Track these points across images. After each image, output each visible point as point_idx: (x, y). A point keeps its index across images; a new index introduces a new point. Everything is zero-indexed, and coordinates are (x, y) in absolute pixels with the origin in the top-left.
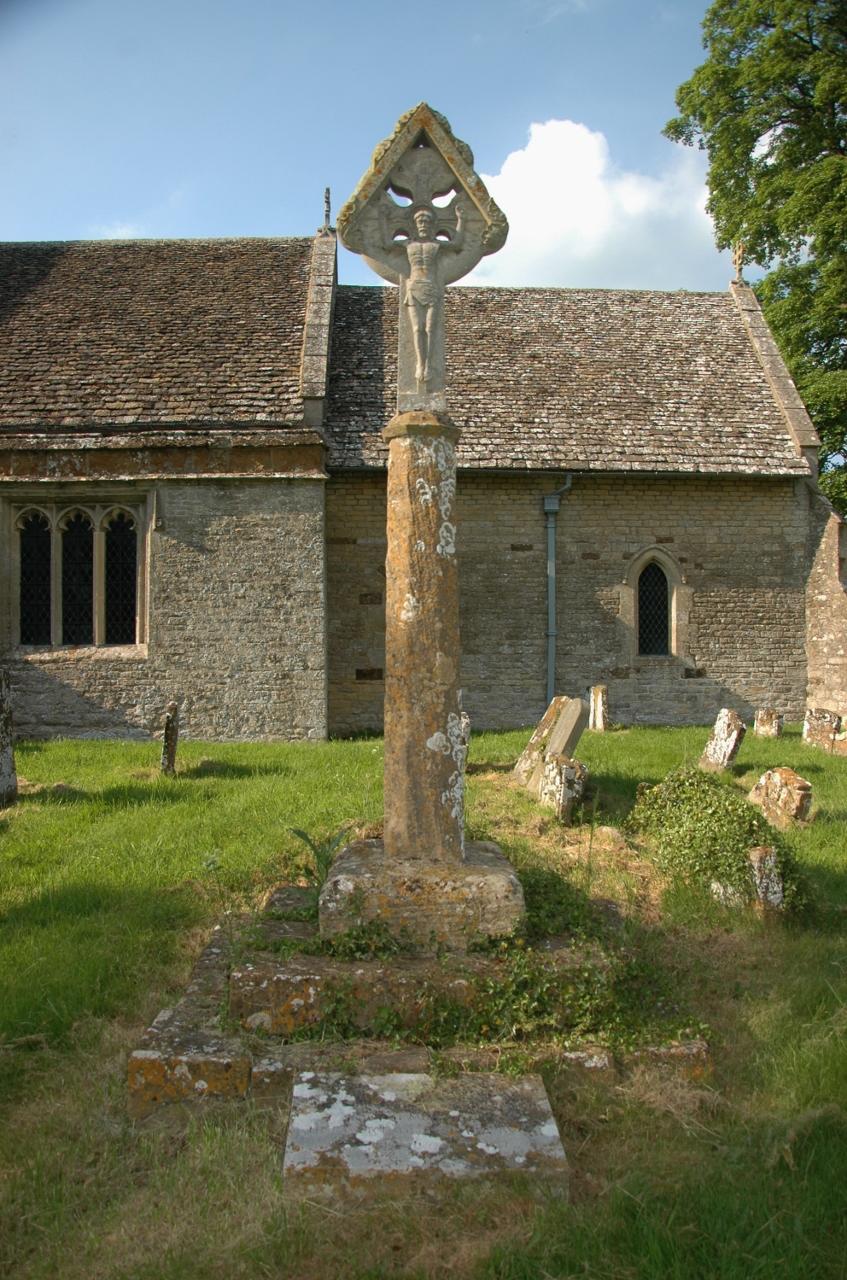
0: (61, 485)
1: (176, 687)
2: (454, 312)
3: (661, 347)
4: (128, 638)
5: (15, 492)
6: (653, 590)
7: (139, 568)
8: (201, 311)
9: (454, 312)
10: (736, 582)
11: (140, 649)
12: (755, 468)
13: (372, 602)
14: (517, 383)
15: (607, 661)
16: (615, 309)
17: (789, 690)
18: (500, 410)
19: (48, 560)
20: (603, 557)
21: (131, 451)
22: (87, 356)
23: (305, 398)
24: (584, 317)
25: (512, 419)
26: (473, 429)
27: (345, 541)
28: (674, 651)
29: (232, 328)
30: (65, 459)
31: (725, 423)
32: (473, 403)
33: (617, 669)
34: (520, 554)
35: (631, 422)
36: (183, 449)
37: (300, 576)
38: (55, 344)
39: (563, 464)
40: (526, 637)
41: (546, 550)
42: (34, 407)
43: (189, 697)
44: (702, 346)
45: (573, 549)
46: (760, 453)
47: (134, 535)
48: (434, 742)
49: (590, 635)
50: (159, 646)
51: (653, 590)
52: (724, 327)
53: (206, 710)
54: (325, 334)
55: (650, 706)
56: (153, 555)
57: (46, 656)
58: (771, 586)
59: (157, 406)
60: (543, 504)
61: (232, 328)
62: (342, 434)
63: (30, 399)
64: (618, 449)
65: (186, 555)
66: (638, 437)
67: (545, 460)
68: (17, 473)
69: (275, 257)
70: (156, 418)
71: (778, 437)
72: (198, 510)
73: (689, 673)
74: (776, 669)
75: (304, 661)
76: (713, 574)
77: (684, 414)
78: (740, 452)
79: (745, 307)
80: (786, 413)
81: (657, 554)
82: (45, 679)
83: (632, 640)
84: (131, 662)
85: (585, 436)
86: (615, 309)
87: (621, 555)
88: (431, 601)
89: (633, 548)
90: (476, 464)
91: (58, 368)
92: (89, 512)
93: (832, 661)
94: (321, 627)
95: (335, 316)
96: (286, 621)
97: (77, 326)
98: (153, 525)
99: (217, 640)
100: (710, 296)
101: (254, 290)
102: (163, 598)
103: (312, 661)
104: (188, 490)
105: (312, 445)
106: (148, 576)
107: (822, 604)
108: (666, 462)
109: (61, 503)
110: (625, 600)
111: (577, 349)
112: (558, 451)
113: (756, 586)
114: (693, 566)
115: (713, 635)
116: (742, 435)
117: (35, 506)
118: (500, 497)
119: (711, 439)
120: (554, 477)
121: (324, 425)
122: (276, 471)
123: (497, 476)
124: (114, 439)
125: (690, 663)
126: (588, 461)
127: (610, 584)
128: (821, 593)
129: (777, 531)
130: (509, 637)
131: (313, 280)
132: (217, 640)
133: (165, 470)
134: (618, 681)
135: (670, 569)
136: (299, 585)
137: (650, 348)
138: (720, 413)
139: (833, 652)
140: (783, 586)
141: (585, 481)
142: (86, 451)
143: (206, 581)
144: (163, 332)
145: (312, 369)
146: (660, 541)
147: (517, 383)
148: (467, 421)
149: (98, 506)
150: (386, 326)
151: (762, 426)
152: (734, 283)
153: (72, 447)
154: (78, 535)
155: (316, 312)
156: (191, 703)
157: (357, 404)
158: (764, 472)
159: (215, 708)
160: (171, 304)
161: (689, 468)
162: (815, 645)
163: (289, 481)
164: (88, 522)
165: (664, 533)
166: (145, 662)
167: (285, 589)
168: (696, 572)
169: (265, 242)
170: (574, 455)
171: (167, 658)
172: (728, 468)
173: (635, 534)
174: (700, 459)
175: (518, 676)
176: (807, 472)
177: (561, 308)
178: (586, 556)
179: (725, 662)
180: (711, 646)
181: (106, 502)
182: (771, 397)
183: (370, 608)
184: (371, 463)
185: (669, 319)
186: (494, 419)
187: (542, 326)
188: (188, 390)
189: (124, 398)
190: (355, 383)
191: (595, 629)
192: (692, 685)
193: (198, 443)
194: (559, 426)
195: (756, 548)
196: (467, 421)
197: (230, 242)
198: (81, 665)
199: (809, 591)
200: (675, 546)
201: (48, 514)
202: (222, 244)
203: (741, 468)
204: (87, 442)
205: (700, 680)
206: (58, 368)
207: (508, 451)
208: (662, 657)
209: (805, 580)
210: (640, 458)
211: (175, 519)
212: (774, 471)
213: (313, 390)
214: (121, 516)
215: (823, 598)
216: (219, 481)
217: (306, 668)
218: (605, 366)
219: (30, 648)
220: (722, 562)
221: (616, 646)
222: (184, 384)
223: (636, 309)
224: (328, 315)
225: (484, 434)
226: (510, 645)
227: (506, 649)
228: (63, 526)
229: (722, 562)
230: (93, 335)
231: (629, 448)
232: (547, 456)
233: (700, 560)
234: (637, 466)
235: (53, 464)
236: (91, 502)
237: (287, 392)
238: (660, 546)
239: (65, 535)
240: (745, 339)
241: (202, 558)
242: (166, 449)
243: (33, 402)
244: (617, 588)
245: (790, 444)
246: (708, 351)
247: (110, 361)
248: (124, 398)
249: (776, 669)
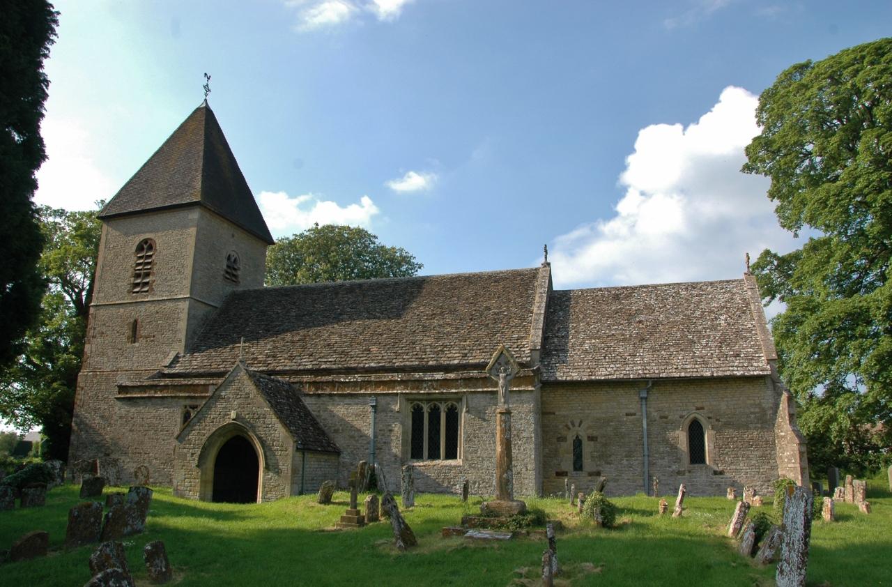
0: (428, 394)
1: (474, 477)
2: (604, 301)
3: (703, 312)
4: (454, 457)
5: (411, 397)
6: (696, 432)
7: (459, 427)
8: (488, 308)
9: (604, 301)
10: (738, 427)
11: (459, 461)
12: (742, 372)
13: (562, 441)
14: (631, 336)
15: (674, 467)
16: (683, 293)
17: (769, 481)
18: (621, 350)
19: (423, 424)
20: (669, 417)
21: (456, 380)
22: (439, 333)
23: (531, 350)
24: (667, 299)
25: (626, 354)
26: (607, 360)
27: (550, 413)
28: (707, 462)
29: (501, 317)
30: (430, 383)
31: (730, 350)
32: (608, 347)
33: (679, 471)
34: (630, 417)
35: (683, 353)
36: (476, 379)
37: (524, 431)
38: (425, 327)
39: (647, 376)
40: (634, 456)
41: (642, 415)
42: (417, 357)
43: (479, 482)
44: (725, 309)
45: (655, 415)
46: (745, 365)
47: (457, 413)
48: (505, 476)
49: (665, 455)
50: (467, 460)
51: (696, 432)
52: (737, 298)
53: (486, 487)
54: (542, 316)
55: (697, 489)
56: (464, 423)
57: (421, 464)
58: (756, 428)
59: (468, 355)
60: (640, 394)
61: (501, 317)
62: (548, 365)
63: (415, 353)
64: (675, 367)
65: (478, 422)
66: (685, 360)
67: (639, 374)
68: (411, 389)
69: (522, 280)
70: (467, 361)
71: (757, 355)
72: (483, 403)
73: (715, 473)
74: (761, 470)
75: (526, 467)
76: (725, 424)
77: (710, 347)
78: (736, 364)
79: (749, 287)
80: (762, 343)
81: (697, 416)
82: (420, 473)
83: (686, 458)
84: (455, 467)
85: (660, 361)
86: (683, 293)
87: (678, 416)
88: (504, 447)
89: (685, 413)
90: (607, 377)
91: (427, 338)
92: (439, 404)
93: (789, 466)
94: (533, 453)
95: (548, 306)
96: (519, 450)
97: (434, 318)
98: (464, 410)
99: (490, 458)
100: (733, 282)
101: (512, 297)
102: (468, 440)
103: (529, 467)
104: (479, 395)
105: (528, 376)
106: (462, 431)
107: (782, 437)
108: (697, 371)
109: (428, 401)
110: (681, 438)
111: (661, 316)
112: (646, 369)
113: (748, 428)
114: (714, 420)
115: (727, 453)
116: (738, 355)
117: (418, 402)
118: (620, 391)
119: (722, 359)
120: (645, 381)
121: (540, 361)
122: (514, 387)
123: (618, 382)
124: (449, 375)
125: (716, 468)
126: (660, 373)
127: (674, 430)
128: (782, 432)
129: (757, 402)
130: (626, 456)
131: (539, 290)
132: (490, 458)
133: (470, 387)
134: (680, 477)
135: (703, 421)
136: (524, 434)
137: (698, 313)
138: (728, 345)
139: (789, 461)
140: (762, 428)
141: (658, 383)
142: (438, 380)
143: (486, 433)
144: (471, 319)
145: (535, 336)
146: (697, 409)
147: (631, 336)
148: (605, 357)
149: (443, 403)
150: (572, 310)
151: (749, 350)
152: (745, 274)
153: (433, 378)
154: (435, 414)
155: (538, 307)
156: (479, 484)
157: (556, 350)
158: (746, 374)
159: (489, 486)
160: (475, 306)
161: (708, 374)
162: (781, 457)
163: (520, 391)
164: (439, 409)
165: (699, 405)
166: (461, 466)
167: (518, 436)
168: (717, 423)
169: (518, 271)
170: (654, 371)
171: (470, 465)
172: (728, 373)
173: (685, 406)
174: (715, 369)
175: (631, 475)
176: (769, 373)
177: (656, 295)
178: (661, 417)
179: (734, 467)
180: (726, 459)
181: (446, 400)
182: (756, 334)
183: (562, 443)
184: (560, 379)
185: (710, 296)
186: (618, 355)
187: (646, 305)
188: (481, 347)
189: (454, 352)
190: (556, 340)
191: (668, 452)
192: (717, 478)
193: (483, 376)
194: (648, 356)
195: (747, 411)
196: (605, 357)
197: (502, 273)
198: (435, 468)
199: (776, 431)
200: (705, 411)
201: (423, 405)
202: (498, 274)
203: (735, 372)
204: (439, 376)
205: (721, 476)
206: (427, 338)
207: (623, 370)
208: (701, 465)
209: (774, 425)
210: (684, 371)
211: (473, 407)
212: (752, 373)
213: (535, 346)
214: (452, 406)
215: (783, 434)
216: (491, 392)
217: (527, 470)
218: (675, 324)
219: (415, 460)
220: (729, 418)
221: (678, 460)
222: (480, 345)
223: (693, 292)
224: (544, 308)
225: (612, 363)
226: (627, 460)
227: (625, 462)
228: (429, 410)
229: (729, 418)
230: (441, 322)
231: (681, 365)
232: (640, 372)
233: (718, 418)
234: (683, 375)
235: (425, 386)
236: (440, 400)
237: (524, 347)
238: (698, 411)
239: (430, 414)
240: (747, 304)
241: (484, 423)
242: (470, 379)
243: (417, 354)
244: (677, 432)
245: (763, 358)
246: (727, 312)
247: (448, 334)
248: (454, 352)
249: (761, 470)
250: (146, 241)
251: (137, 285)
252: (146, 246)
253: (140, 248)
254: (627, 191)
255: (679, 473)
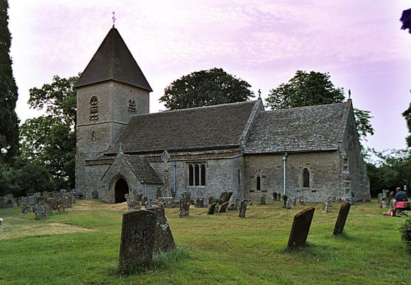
109: (194, 163)
135: (309, 170)
242: (208, 154)
250: (94, 97)
251: (92, 117)
252: (94, 99)
253: (92, 101)
254: (116, 30)
255: (298, 191)
